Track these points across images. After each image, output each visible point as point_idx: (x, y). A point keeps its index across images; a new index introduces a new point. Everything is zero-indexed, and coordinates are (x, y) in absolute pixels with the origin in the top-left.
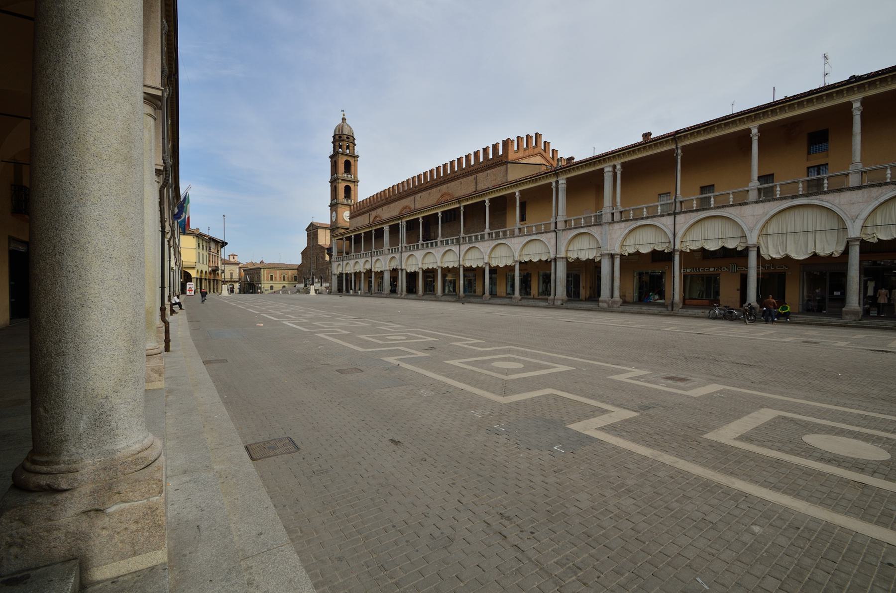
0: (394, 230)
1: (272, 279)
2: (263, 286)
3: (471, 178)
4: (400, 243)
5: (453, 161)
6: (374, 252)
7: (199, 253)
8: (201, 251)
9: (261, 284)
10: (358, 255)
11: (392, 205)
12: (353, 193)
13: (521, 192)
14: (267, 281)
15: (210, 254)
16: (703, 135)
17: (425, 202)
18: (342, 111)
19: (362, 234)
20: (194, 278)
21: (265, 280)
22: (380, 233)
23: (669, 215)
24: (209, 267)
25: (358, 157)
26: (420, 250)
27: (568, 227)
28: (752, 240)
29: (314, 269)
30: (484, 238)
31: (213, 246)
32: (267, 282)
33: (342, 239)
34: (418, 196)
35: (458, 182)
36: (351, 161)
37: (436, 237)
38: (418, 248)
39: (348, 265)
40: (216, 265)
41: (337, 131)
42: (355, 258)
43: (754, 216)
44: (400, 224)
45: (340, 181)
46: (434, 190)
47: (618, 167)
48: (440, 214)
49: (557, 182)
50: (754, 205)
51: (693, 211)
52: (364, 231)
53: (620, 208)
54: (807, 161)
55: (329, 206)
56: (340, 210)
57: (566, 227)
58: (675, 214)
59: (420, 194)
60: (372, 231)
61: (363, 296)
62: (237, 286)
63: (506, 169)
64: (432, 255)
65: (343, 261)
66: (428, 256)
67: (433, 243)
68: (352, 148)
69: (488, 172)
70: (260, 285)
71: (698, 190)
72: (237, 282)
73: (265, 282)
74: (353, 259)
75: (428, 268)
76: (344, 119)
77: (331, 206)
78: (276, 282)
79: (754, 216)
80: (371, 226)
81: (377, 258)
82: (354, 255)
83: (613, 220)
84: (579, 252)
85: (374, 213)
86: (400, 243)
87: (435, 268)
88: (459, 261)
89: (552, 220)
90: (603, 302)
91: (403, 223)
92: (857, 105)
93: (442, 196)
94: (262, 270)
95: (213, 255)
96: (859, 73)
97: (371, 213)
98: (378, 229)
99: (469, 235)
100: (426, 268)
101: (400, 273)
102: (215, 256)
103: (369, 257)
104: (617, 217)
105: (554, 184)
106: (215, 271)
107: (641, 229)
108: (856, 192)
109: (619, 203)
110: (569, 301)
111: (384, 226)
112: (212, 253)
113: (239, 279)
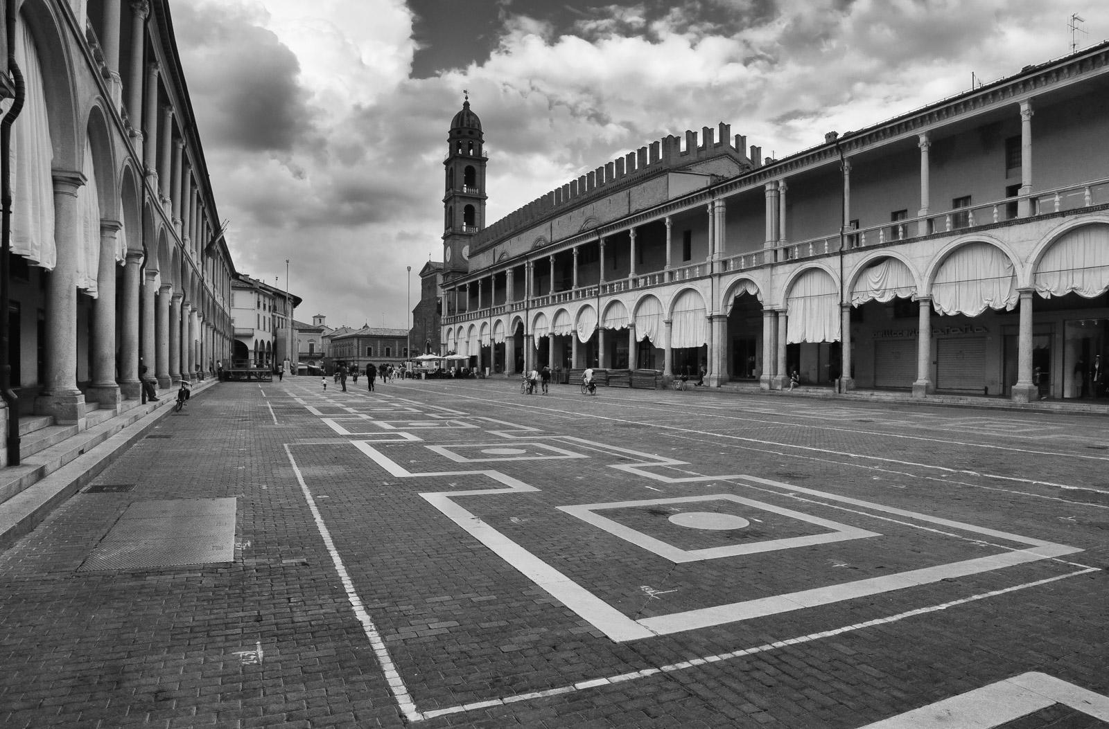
0: (519, 274)
1: (369, 354)
3: (623, 194)
4: (526, 295)
5: (591, 172)
6: (494, 309)
7: (259, 315)
8: (261, 311)
10: (487, 311)
11: (523, 236)
12: (477, 216)
13: (671, 217)
14: (363, 355)
16: (1044, 83)
17: (564, 229)
18: (465, 92)
19: (667, 220)
21: (360, 355)
22: (501, 279)
23: (835, 254)
26: (574, 301)
27: (935, 232)
28: (922, 292)
29: (430, 337)
30: (628, 288)
31: (279, 303)
32: (363, 359)
33: (453, 290)
34: (555, 222)
35: (605, 201)
36: (474, 166)
37: (663, 263)
38: (571, 298)
42: (481, 316)
43: (923, 257)
44: (526, 266)
46: (576, 212)
47: (781, 184)
49: (713, 203)
50: (923, 242)
51: (1054, 215)
52: (469, 281)
54: (1007, 178)
55: (443, 238)
57: (932, 231)
58: (842, 253)
59: (557, 219)
63: (666, 182)
64: (589, 309)
65: (490, 316)
67: (655, 276)
69: (644, 185)
71: (1004, 192)
74: (468, 320)
75: (622, 328)
76: (466, 105)
78: (394, 359)
79: (923, 257)
81: (557, 308)
83: (776, 260)
84: (808, 301)
85: (499, 249)
86: (526, 295)
87: (625, 327)
89: (707, 260)
90: (764, 381)
91: (529, 265)
92: (1024, 107)
93: (586, 221)
95: (278, 318)
96: (854, 130)
97: (496, 248)
99: (659, 272)
101: (525, 340)
103: (487, 317)
104: (781, 257)
105: (710, 207)
107: (970, 252)
108: (1028, 225)
110: (731, 380)
111: (506, 269)
112: (277, 315)
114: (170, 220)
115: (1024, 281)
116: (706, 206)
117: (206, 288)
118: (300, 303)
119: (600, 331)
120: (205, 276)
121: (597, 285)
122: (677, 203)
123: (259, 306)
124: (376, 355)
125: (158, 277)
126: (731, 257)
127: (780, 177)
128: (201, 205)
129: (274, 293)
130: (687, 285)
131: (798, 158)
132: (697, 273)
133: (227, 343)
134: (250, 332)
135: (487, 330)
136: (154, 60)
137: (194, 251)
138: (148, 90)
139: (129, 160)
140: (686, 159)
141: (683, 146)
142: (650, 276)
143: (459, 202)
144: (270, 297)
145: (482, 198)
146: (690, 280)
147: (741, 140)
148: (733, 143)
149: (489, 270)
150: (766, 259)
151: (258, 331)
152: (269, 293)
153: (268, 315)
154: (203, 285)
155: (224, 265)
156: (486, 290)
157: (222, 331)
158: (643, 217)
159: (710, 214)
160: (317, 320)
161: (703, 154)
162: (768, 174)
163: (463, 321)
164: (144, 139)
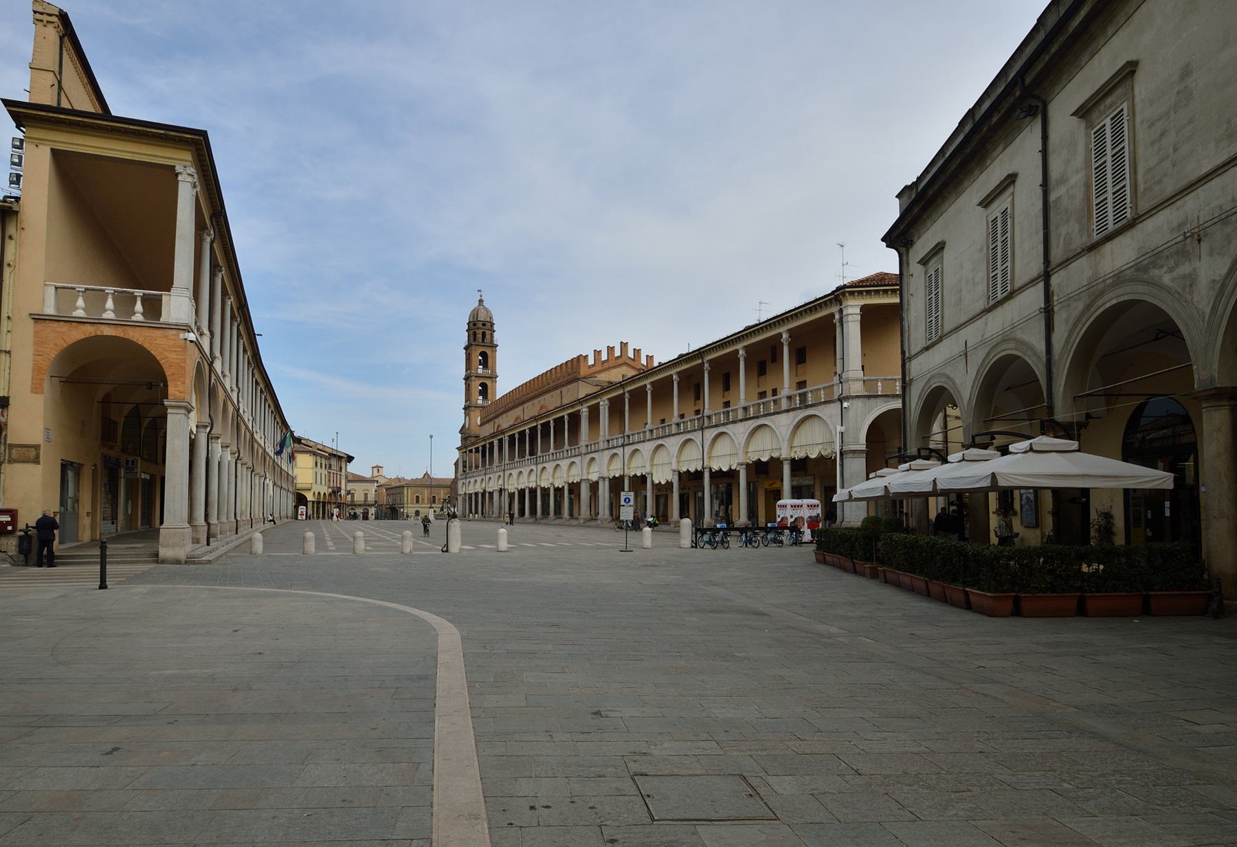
2: (406, 511)
6: (540, 457)
7: (316, 472)
9: (403, 508)
11: (509, 414)
12: (489, 391)
13: (652, 383)
14: (412, 503)
15: (330, 473)
18: (479, 291)
19: (785, 336)
20: (310, 501)
21: (409, 502)
22: (575, 419)
24: (329, 487)
25: (497, 346)
31: (334, 462)
32: (412, 505)
33: (466, 452)
39: (545, 470)
40: (338, 486)
41: (472, 317)
45: (473, 378)
48: (527, 431)
53: (742, 403)
55: (464, 409)
56: (472, 414)
60: (537, 426)
61: (480, 521)
62: (372, 511)
64: (727, 436)
65: (537, 464)
66: (760, 435)
68: (490, 336)
69: (569, 387)
70: (402, 510)
71: (693, 413)
72: (372, 505)
73: (409, 505)
75: (688, 470)
76: (481, 301)
77: (465, 409)
78: (424, 506)
80: (536, 420)
82: (553, 454)
88: (536, 481)
94: (405, 489)
95: (333, 473)
98: (543, 423)
100: (685, 470)
102: (337, 474)
105: (837, 316)
106: (336, 491)
107: (813, 420)
109: (607, 433)
113: (376, 502)
114: (220, 375)
115: (551, 481)
116: (832, 315)
117: (256, 441)
118: (352, 460)
119: (785, 462)
120: (241, 405)
121: (622, 435)
122: (670, 365)
123: (316, 465)
124: (423, 502)
125: (193, 415)
126: (752, 403)
127: (606, 398)
128: (236, 321)
129: (330, 454)
130: (722, 429)
131: (797, 311)
132: (772, 408)
133: (290, 495)
134: (309, 486)
135: (533, 477)
136: (241, 335)
137: (227, 373)
138: (213, 298)
139: (200, 357)
140: (593, 370)
141: (591, 361)
142: (723, 413)
143: (474, 381)
144: (326, 458)
145: (493, 377)
146: (765, 415)
147: (637, 352)
148: (631, 354)
149: (535, 419)
150: (782, 406)
151: (316, 485)
152: (325, 454)
153: (324, 472)
154: (253, 438)
155: (275, 418)
156: (545, 435)
157: (287, 488)
158: (762, 330)
159: (838, 324)
160: (376, 470)
161: (606, 365)
162: (828, 303)
163: (546, 462)
164: (211, 335)
